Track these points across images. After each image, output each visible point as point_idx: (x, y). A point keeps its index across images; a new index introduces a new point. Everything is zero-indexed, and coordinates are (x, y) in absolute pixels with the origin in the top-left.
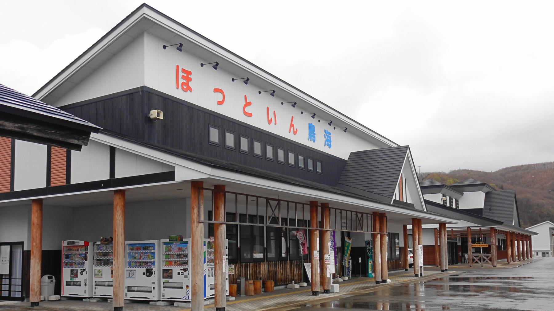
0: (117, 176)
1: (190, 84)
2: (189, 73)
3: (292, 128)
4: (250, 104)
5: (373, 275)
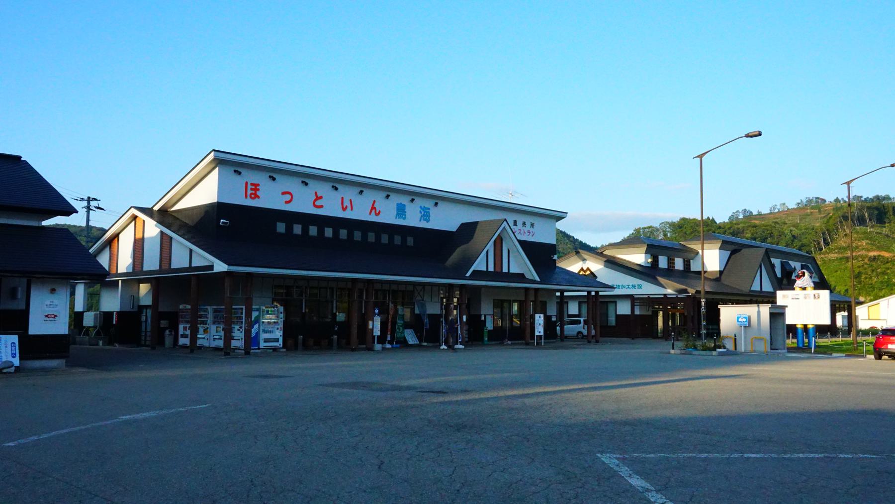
0: (193, 265)
1: (258, 193)
2: (256, 185)
3: (374, 211)
4: (321, 197)
5: (855, 283)
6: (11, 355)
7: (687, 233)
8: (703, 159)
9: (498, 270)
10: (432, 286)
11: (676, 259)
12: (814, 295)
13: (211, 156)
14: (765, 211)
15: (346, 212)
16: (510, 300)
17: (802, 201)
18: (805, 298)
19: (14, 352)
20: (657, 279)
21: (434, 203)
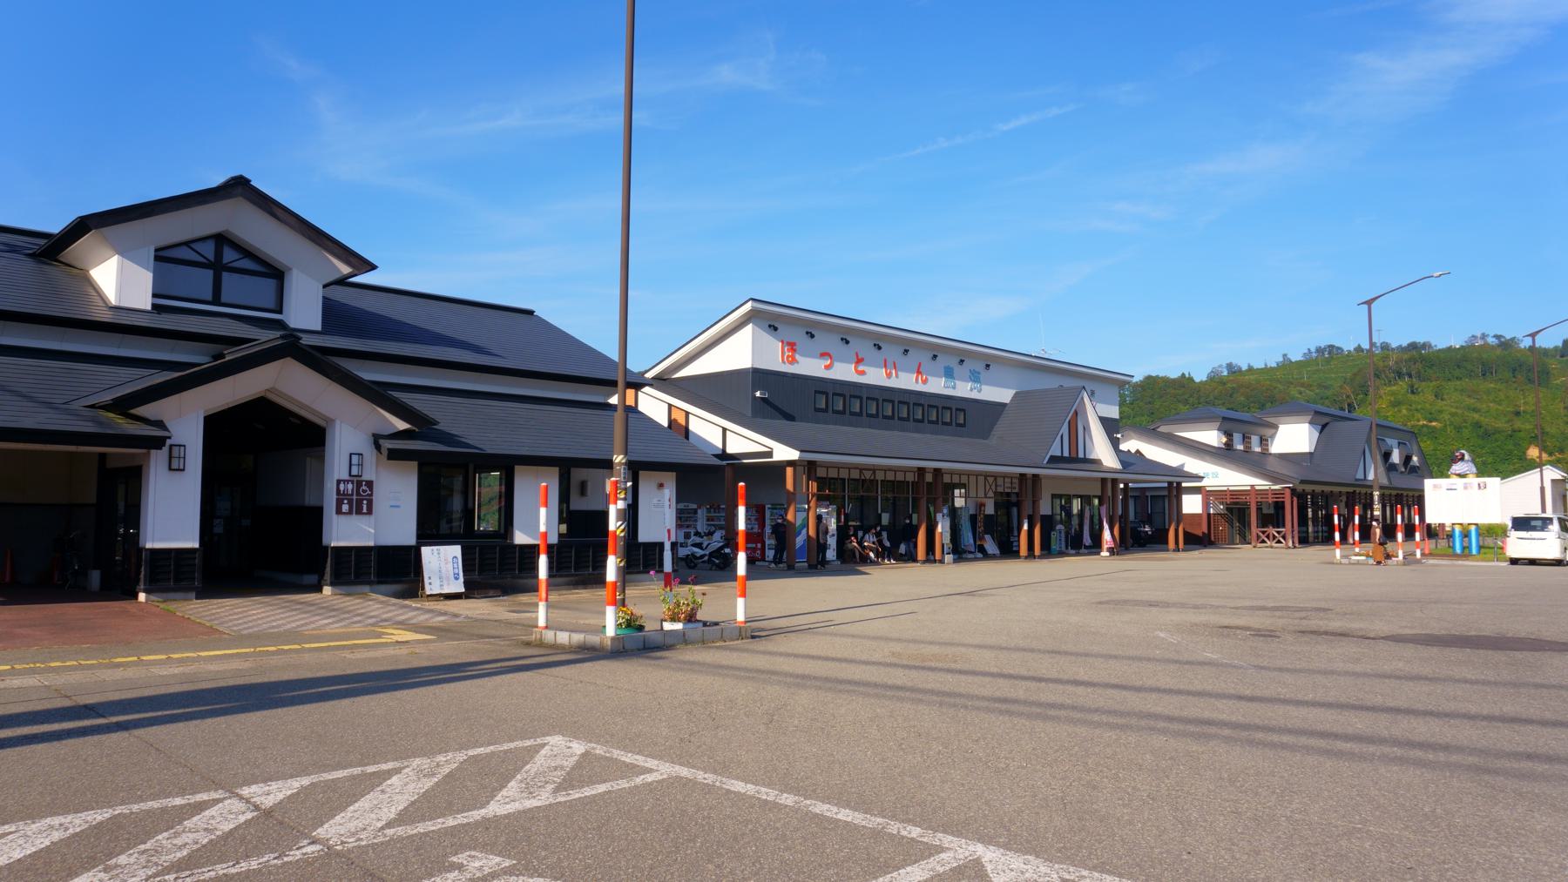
6: (453, 576)
7: (1270, 404)
8: (55, 226)
9: (1074, 455)
10: (905, 472)
11: (1252, 437)
12: (1479, 485)
13: (748, 306)
14: (1258, 365)
15: (890, 380)
16: (1090, 496)
17: (1309, 350)
18: (1465, 488)
19: (456, 571)
20: (1122, 462)
21: (958, 360)
